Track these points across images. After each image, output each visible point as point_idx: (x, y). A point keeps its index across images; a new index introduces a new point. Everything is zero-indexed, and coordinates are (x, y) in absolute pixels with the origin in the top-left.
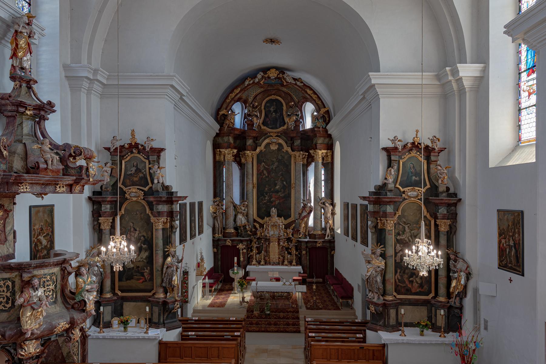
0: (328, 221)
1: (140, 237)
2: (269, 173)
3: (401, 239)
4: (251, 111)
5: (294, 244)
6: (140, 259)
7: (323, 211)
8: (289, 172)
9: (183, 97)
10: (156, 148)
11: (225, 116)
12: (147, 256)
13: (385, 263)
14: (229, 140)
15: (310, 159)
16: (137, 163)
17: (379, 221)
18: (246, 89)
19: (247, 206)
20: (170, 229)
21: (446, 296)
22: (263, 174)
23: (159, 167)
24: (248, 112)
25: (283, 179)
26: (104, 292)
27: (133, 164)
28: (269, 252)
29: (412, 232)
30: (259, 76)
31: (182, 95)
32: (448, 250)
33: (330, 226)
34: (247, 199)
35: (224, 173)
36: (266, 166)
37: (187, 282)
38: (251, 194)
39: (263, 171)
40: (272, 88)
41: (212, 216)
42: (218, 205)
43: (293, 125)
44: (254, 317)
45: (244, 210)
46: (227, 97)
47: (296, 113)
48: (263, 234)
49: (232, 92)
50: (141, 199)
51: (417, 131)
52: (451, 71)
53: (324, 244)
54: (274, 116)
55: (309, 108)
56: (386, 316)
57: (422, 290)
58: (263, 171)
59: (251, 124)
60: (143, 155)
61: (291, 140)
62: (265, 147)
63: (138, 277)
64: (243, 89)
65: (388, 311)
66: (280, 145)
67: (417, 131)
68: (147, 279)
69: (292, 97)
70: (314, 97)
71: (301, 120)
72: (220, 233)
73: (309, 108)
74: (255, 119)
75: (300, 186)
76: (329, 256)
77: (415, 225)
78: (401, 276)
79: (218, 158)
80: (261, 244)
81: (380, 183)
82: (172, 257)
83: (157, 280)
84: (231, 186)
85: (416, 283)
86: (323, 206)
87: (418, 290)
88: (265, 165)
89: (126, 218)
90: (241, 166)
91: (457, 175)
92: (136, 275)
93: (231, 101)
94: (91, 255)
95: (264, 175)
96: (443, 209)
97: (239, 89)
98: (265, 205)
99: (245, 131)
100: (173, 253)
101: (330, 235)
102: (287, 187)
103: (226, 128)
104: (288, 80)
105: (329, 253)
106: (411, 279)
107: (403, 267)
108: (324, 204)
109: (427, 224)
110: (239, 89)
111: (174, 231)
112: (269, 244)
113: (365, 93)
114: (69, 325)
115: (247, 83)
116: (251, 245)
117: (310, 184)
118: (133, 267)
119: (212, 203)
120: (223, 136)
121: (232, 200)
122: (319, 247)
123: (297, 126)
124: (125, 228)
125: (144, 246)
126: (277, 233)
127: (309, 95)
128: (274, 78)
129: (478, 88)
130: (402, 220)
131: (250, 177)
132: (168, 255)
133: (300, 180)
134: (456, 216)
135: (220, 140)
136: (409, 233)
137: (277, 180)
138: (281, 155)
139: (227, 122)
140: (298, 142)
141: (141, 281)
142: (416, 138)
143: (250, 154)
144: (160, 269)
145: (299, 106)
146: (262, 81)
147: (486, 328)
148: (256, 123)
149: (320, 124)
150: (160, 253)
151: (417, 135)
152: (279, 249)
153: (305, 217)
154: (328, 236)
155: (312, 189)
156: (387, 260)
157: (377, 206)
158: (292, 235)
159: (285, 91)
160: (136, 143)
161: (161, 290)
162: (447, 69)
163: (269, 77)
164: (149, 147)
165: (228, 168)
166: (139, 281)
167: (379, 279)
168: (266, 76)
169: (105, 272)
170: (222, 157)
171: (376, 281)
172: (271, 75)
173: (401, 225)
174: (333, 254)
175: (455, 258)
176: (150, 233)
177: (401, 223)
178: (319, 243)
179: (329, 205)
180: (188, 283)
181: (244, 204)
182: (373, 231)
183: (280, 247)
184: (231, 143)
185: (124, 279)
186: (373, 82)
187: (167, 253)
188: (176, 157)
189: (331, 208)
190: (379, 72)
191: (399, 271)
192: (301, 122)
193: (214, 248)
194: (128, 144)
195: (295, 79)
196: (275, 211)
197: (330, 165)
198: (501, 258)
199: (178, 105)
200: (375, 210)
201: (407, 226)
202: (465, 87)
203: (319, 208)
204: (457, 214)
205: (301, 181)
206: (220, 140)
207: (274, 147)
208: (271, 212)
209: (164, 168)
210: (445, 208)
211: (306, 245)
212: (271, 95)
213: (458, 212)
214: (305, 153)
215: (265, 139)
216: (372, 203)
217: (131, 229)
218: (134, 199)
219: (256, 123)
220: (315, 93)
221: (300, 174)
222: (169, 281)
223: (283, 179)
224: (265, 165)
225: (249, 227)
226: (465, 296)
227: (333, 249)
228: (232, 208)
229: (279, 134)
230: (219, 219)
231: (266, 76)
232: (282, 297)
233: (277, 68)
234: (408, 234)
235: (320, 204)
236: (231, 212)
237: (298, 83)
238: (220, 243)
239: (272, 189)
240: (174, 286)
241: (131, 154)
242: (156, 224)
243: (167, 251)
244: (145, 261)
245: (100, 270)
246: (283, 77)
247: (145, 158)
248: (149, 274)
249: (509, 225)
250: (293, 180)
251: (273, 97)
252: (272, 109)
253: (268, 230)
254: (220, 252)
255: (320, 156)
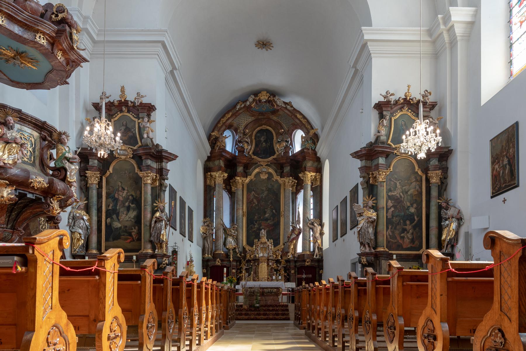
0: (317, 241)
1: (129, 196)
2: (259, 202)
3: (392, 195)
4: (242, 137)
5: (283, 266)
6: (128, 219)
7: (311, 233)
8: (278, 201)
9: (175, 71)
10: (146, 104)
11: (216, 139)
12: (135, 215)
13: (377, 214)
14: (220, 163)
15: (299, 185)
16: (126, 123)
17: (371, 176)
18: (237, 114)
19: (237, 230)
20: (160, 188)
21: (437, 247)
22: (253, 202)
23: (148, 121)
24: (239, 138)
25: (272, 207)
26: (90, 248)
27: (123, 123)
28: (259, 273)
29: (404, 188)
30: (251, 99)
31: (174, 68)
32: (439, 199)
33: (319, 245)
34: (236, 222)
35: (215, 203)
36: (256, 195)
37: (176, 262)
38: (241, 220)
39: (253, 200)
40: (262, 117)
41: (202, 236)
42: (208, 226)
43: (283, 151)
44: (243, 309)
45: (234, 233)
46: (219, 122)
47: (286, 140)
48: (252, 256)
49: (223, 117)
50: (130, 157)
51: (409, 86)
52: (443, 18)
53: (313, 263)
54: (264, 145)
55: (299, 135)
56: (378, 268)
57: (413, 246)
58: (253, 200)
59: (241, 151)
60: (133, 114)
61: (281, 169)
62: (255, 176)
63: (126, 237)
64: (234, 113)
65: (379, 262)
66: (270, 174)
67: (409, 86)
68: (134, 239)
69: (282, 126)
70: (304, 121)
71: (291, 146)
72: (209, 254)
73: (299, 135)
74: (246, 145)
75: (289, 211)
76: (317, 275)
77: (406, 182)
78: (393, 232)
79: (208, 182)
80: (251, 266)
81: (372, 139)
82: (161, 212)
83: (145, 235)
84: (221, 209)
85: (407, 239)
86: (311, 226)
87: (409, 246)
88: (255, 194)
89: (115, 178)
90: (232, 194)
91: (448, 126)
92: (124, 235)
93: (222, 126)
94: (77, 207)
95: (254, 203)
96: (434, 160)
97: (231, 114)
98: (254, 233)
99: (236, 156)
100: (162, 208)
101: (318, 255)
102: (277, 215)
103: (217, 149)
104: (278, 103)
105: (317, 272)
106: (402, 235)
107: (394, 223)
108: (312, 224)
109: (419, 180)
110: (231, 114)
111: (163, 189)
112: (258, 264)
113: (355, 66)
114: (47, 185)
115: (238, 107)
116: (240, 266)
117: (299, 205)
118: (121, 227)
119: (202, 224)
120: (214, 161)
121: (223, 221)
122: (307, 266)
123: (287, 152)
124: (113, 188)
125: (132, 206)
126: (266, 255)
127: (299, 119)
128: (265, 100)
129: (469, 36)
130: (393, 176)
131: (241, 203)
132: (157, 211)
133: (290, 206)
134: (447, 171)
135: (211, 164)
136: (400, 189)
137: (267, 208)
138: (271, 184)
139: (218, 144)
140: (287, 169)
141: (129, 240)
142: (408, 93)
143: (240, 181)
144: (148, 224)
145: (290, 134)
146: (253, 104)
147: (471, 330)
148: (247, 149)
149: (309, 145)
150: (149, 209)
151: (408, 90)
152: (268, 269)
153: (293, 239)
154: (316, 256)
155: (301, 209)
156: (379, 212)
157: (368, 161)
158: (281, 257)
159: (275, 120)
160: (125, 100)
161: (149, 246)
162: (439, 16)
163: (260, 101)
164: (139, 103)
165: (218, 190)
166: (126, 241)
167: (371, 230)
168: (257, 98)
169: (91, 228)
170: (213, 182)
171: (368, 232)
172: (262, 98)
173: (393, 181)
174: (321, 274)
175: (446, 205)
176: (138, 192)
177: (393, 180)
178: (308, 262)
179: (318, 225)
180: (177, 263)
181: (234, 227)
182: (365, 186)
183: (270, 268)
184: (222, 167)
185: (111, 239)
186: (366, 37)
187: (156, 209)
188: (167, 130)
189: (319, 228)
190: (371, 26)
191: (390, 227)
192: (291, 148)
193: (203, 269)
194: (117, 101)
195: (285, 103)
196: (265, 233)
197: (319, 188)
198: (494, 186)
199: (169, 83)
200: (367, 165)
201: (398, 182)
202: (457, 35)
203: (308, 229)
204: (448, 168)
205: (290, 206)
206: (211, 164)
207: (264, 177)
208: (261, 234)
209: (154, 121)
210: (436, 160)
211: (295, 264)
212: (261, 125)
213: (449, 166)
214: (295, 180)
215: (255, 168)
216: (364, 158)
217: (119, 188)
218: (123, 157)
219: (247, 149)
220: (304, 117)
221: (289, 199)
222: (157, 236)
223: (272, 207)
224: (255, 194)
225: (238, 250)
226: (457, 243)
227: (321, 268)
228: (222, 231)
229: (269, 163)
230: (209, 240)
231: (257, 98)
232: (272, 293)
233: (268, 91)
234: (400, 190)
235: (309, 225)
236: (222, 236)
237: (288, 107)
238: (209, 263)
239: (262, 218)
240: (163, 241)
241: (120, 113)
242: (145, 179)
243: (157, 206)
244: (133, 220)
245: (86, 224)
246: (274, 99)
247: (135, 117)
248: (137, 234)
249: (503, 146)
250: (283, 209)
251: (264, 127)
252: (262, 139)
253: (258, 251)
254: (209, 272)
255: (309, 179)
